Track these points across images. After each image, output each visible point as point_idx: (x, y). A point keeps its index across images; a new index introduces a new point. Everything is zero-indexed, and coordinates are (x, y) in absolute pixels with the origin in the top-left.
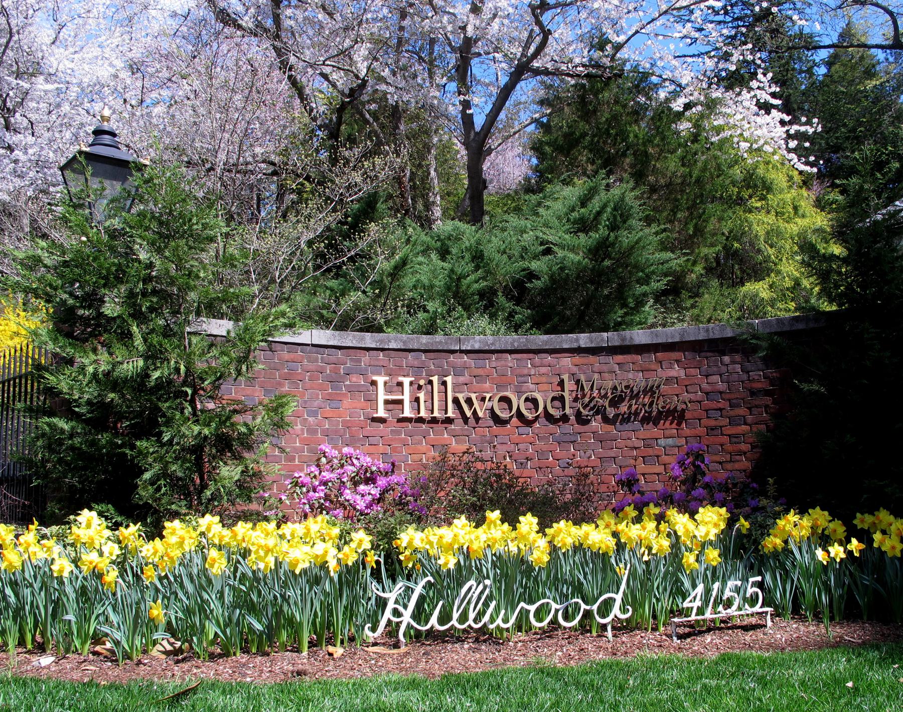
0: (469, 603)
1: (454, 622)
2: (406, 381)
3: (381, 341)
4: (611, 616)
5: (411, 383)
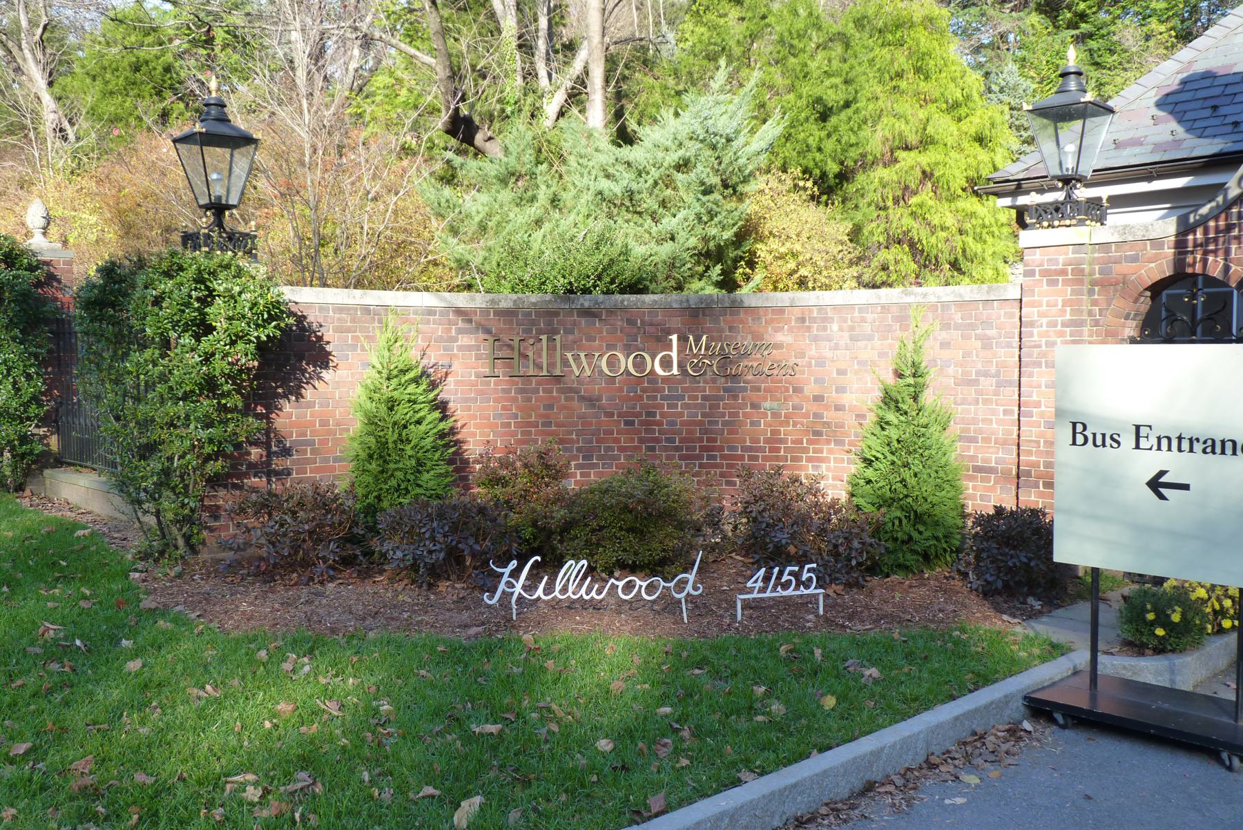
0: (568, 580)
1: (557, 593)
4: (686, 592)
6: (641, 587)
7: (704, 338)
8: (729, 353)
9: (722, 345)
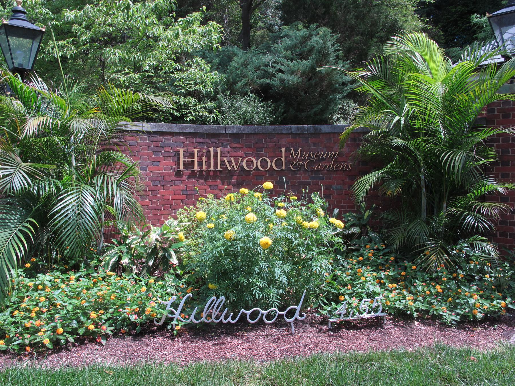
2: (196, 151)
3: (182, 128)
5: (198, 152)
6: (263, 315)
7: (300, 149)
8: (314, 158)
9: (309, 154)
